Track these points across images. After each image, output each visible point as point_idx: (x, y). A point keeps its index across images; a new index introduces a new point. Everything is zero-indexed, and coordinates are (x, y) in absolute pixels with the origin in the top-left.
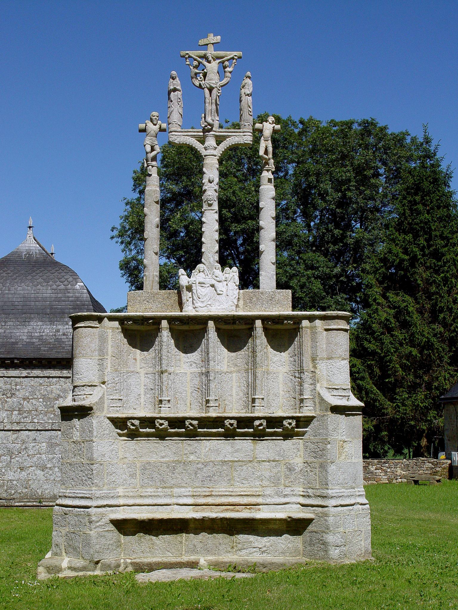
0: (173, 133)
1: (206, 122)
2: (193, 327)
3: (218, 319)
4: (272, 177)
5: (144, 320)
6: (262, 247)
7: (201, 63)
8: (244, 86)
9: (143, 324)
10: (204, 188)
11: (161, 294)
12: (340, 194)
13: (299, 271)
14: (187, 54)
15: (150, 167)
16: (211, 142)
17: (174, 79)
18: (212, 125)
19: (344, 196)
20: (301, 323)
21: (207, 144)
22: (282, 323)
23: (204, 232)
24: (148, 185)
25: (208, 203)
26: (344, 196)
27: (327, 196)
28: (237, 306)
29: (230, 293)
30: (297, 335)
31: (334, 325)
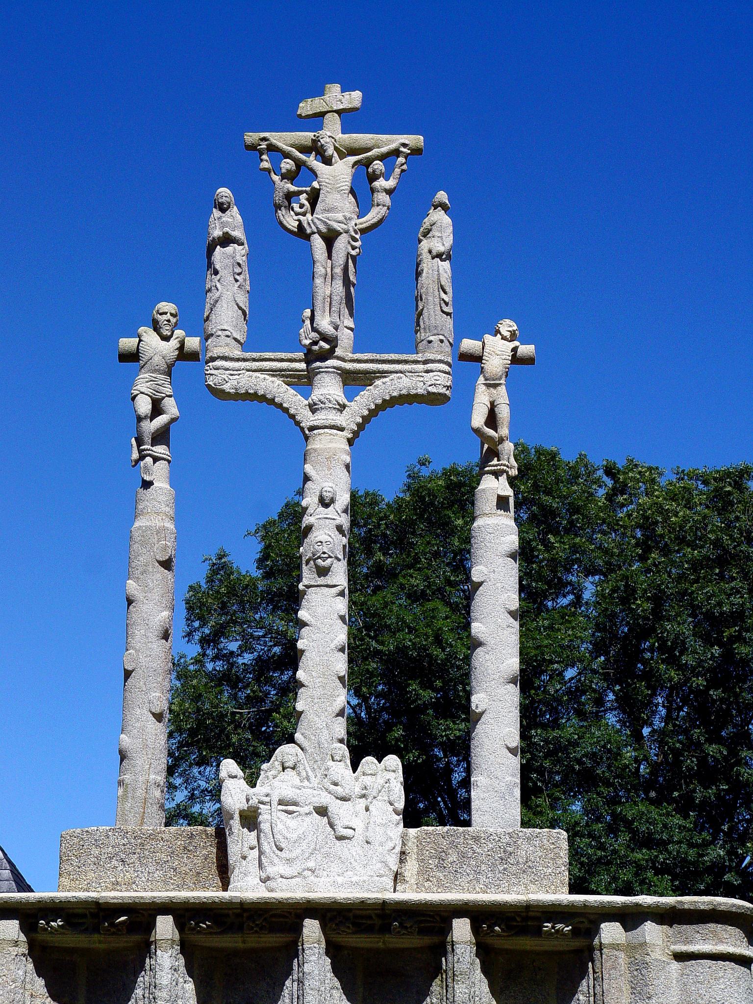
0: (218, 363)
1: (314, 329)
2: (254, 941)
3: (336, 916)
4: (509, 492)
5: (95, 915)
6: (478, 701)
7: (304, 163)
8: (429, 231)
9: (96, 929)
10: (307, 520)
11: (166, 836)
12: (716, 650)
13: (615, 852)
14: (264, 139)
15: (149, 460)
16: (328, 387)
17: (223, 210)
18: (333, 341)
19: (728, 655)
20: (596, 931)
21: (317, 394)
22: (538, 932)
23: (302, 651)
24: (142, 513)
25: (317, 567)
26: (728, 655)
27: (682, 653)
28: (397, 877)
29: (377, 835)
30: (583, 973)
31: (704, 939)
